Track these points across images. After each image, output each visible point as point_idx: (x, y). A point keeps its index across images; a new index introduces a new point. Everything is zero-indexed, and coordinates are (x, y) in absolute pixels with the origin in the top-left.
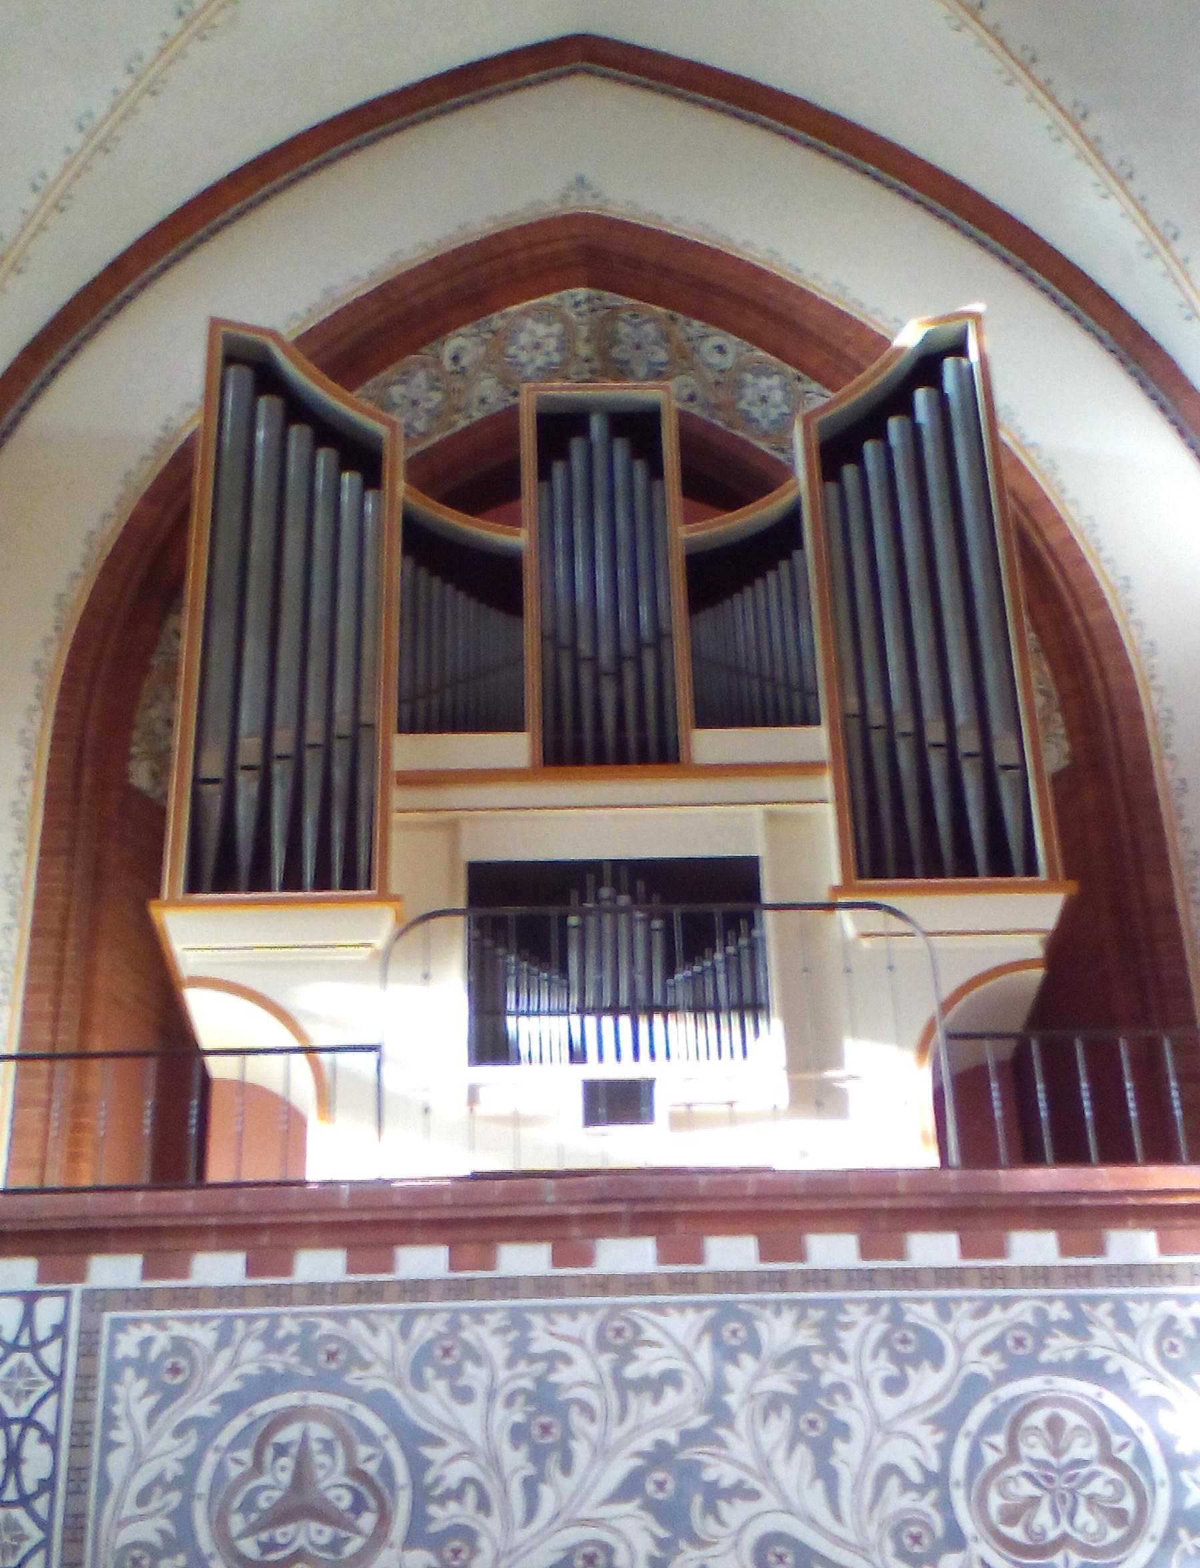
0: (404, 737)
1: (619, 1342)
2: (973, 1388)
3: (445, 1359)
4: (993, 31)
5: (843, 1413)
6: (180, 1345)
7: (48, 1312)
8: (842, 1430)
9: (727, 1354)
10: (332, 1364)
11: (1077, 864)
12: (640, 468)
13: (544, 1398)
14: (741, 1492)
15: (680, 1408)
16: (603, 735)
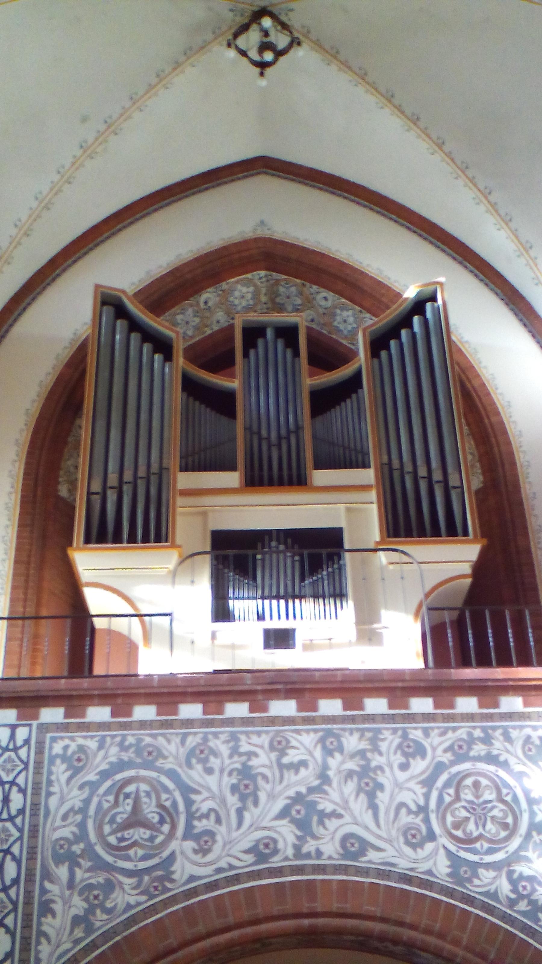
0: (183, 474)
1: (280, 747)
2: (440, 768)
3: (201, 755)
4: (449, 155)
5: (381, 779)
6: (81, 748)
7: (22, 733)
8: (380, 787)
9: (328, 752)
10: (150, 757)
12: (289, 352)
13: (246, 772)
16: (273, 472)
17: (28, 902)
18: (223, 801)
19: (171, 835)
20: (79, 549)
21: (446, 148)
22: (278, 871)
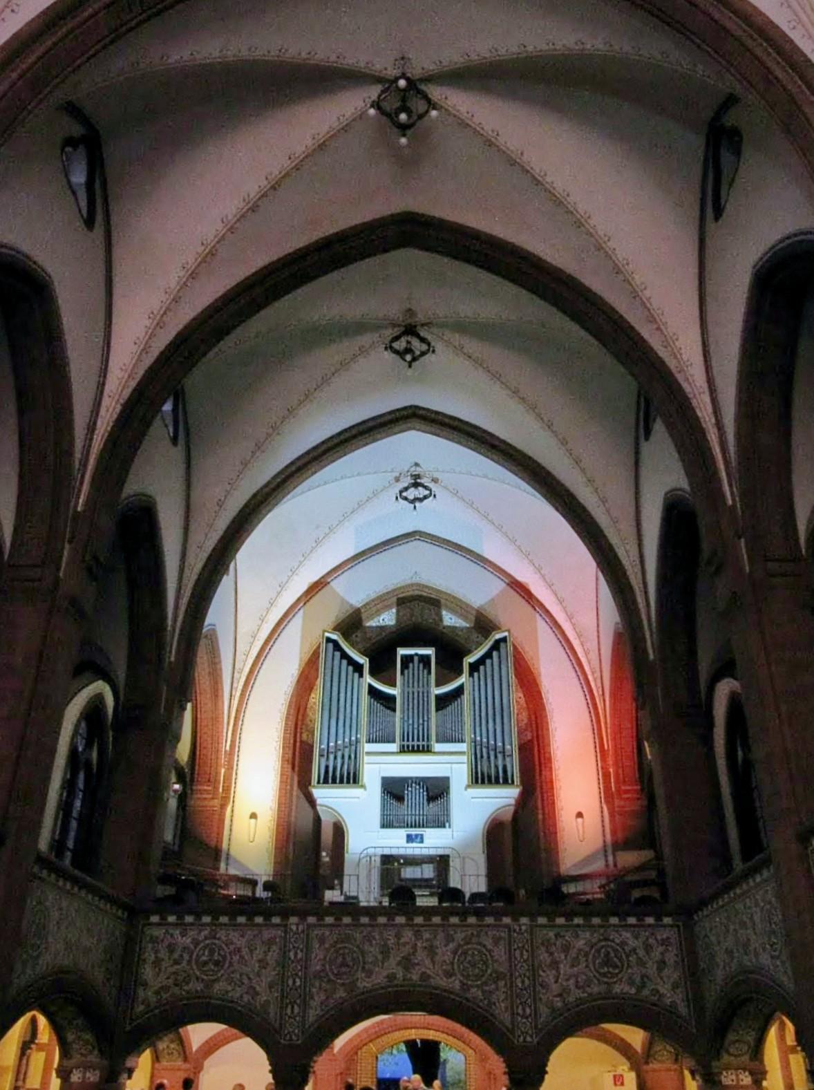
0: (369, 744)
1: (398, 936)
2: (460, 946)
3: (368, 938)
4: (519, 547)
5: (437, 951)
6: (323, 934)
7: (301, 927)
8: (437, 954)
9: (417, 939)
10: (348, 938)
11: (523, 782)
12: (426, 672)
13: (386, 945)
14: (418, 964)
15: (407, 949)
16: (416, 746)
17: (305, 993)
18: (376, 958)
19: (357, 970)
20: (314, 787)
21: (517, 543)
22: (396, 986)
